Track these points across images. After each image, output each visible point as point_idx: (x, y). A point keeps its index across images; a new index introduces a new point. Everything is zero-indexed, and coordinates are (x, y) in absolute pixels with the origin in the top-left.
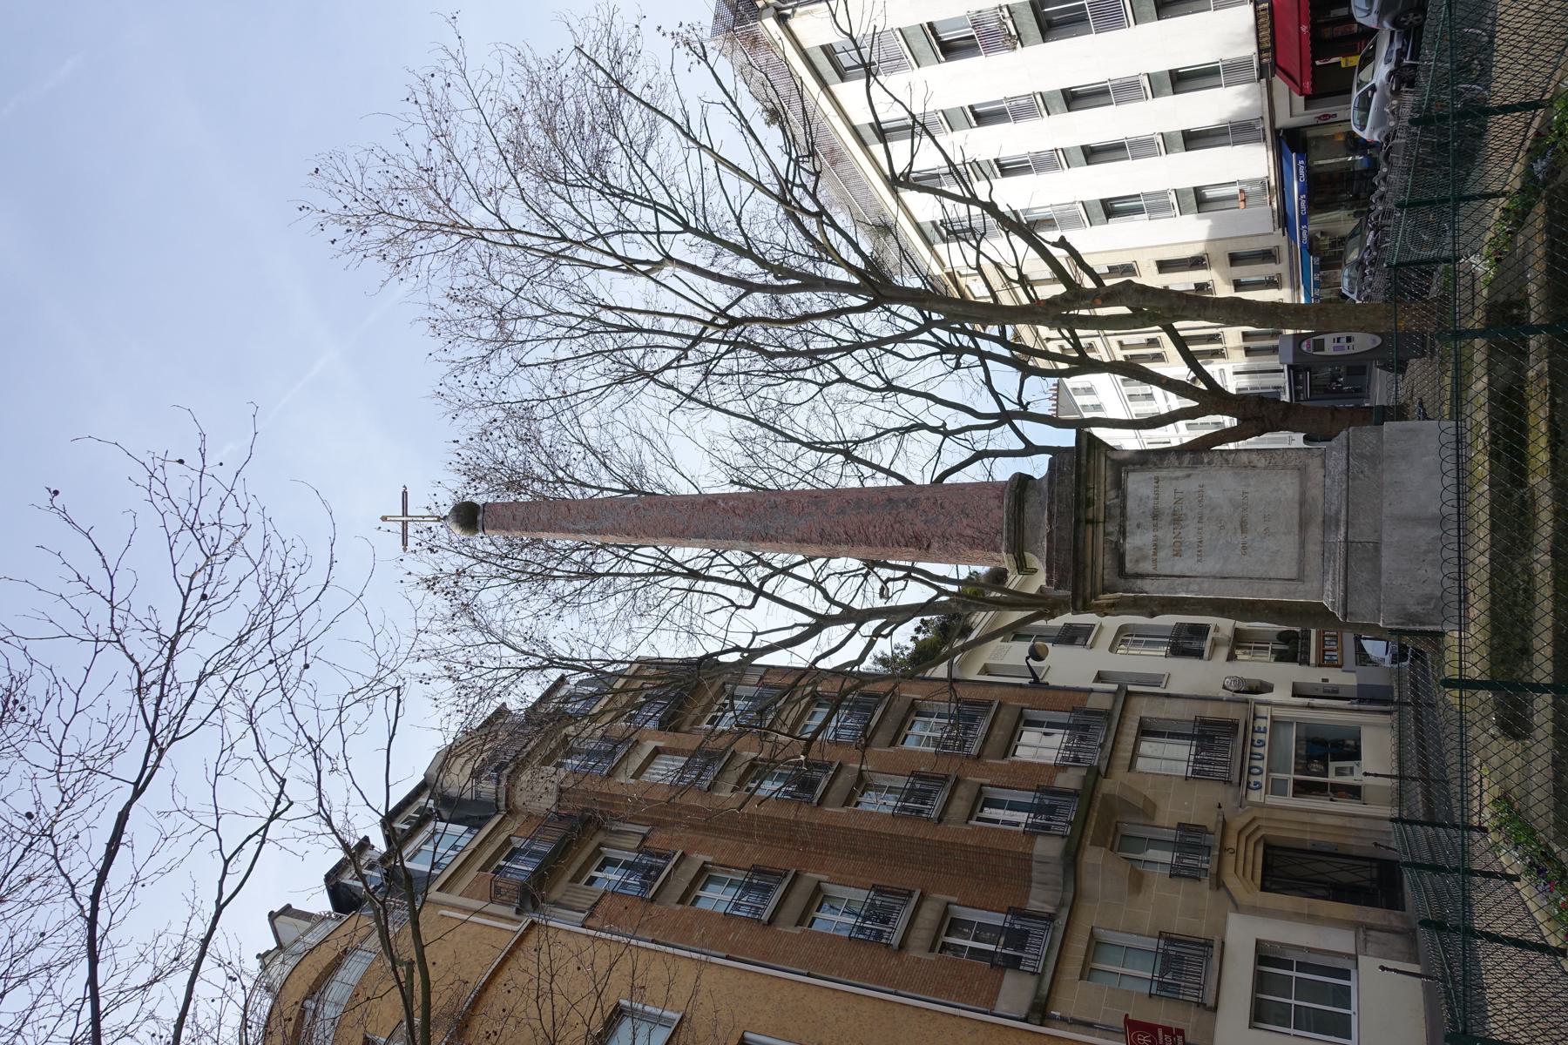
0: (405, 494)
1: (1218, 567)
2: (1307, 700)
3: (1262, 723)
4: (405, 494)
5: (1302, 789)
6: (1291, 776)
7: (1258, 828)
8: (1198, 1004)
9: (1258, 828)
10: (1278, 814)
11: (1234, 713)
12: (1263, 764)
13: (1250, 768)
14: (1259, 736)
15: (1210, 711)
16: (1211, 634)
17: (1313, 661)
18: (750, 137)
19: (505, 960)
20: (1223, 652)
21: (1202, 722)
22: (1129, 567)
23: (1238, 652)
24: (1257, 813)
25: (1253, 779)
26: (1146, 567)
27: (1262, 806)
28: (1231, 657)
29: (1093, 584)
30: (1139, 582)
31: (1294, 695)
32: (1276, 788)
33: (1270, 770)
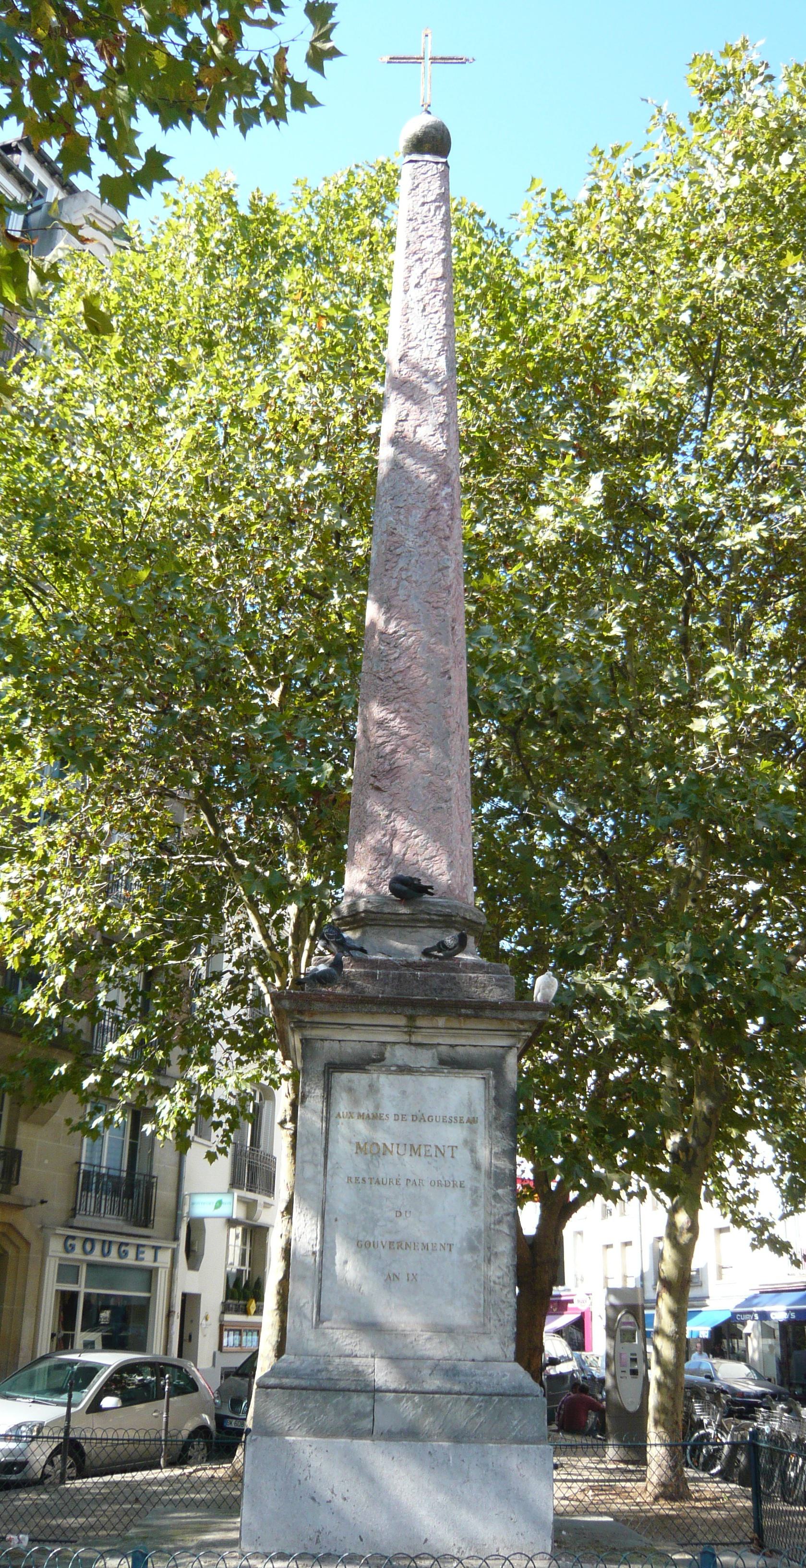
0: (461, 61)
1: (341, 1207)
2: (177, 1309)
3: (148, 1255)
4: (461, 61)
5: (67, 1301)
6: (82, 1289)
7: (17, 1247)
8: (74, 1209)
9: (17, 1247)
10: (33, 1272)
11: (161, 1219)
12: (96, 1256)
13: (92, 1241)
14: (132, 1252)
15: (163, 1195)
16: (261, 1198)
17: (228, 1317)
18: (296, 1382)
19: (327, 1139)
20: (238, 1213)
21: (150, 1185)
22: (342, 1078)
23: (239, 1230)
24: (35, 1246)
25: (78, 1245)
26: (342, 1105)
27: (44, 1253)
28: (231, 1222)
29: (315, 1025)
30: (319, 1092)
31: (184, 1295)
32: (68, 1271)
33: (91, 1266)
